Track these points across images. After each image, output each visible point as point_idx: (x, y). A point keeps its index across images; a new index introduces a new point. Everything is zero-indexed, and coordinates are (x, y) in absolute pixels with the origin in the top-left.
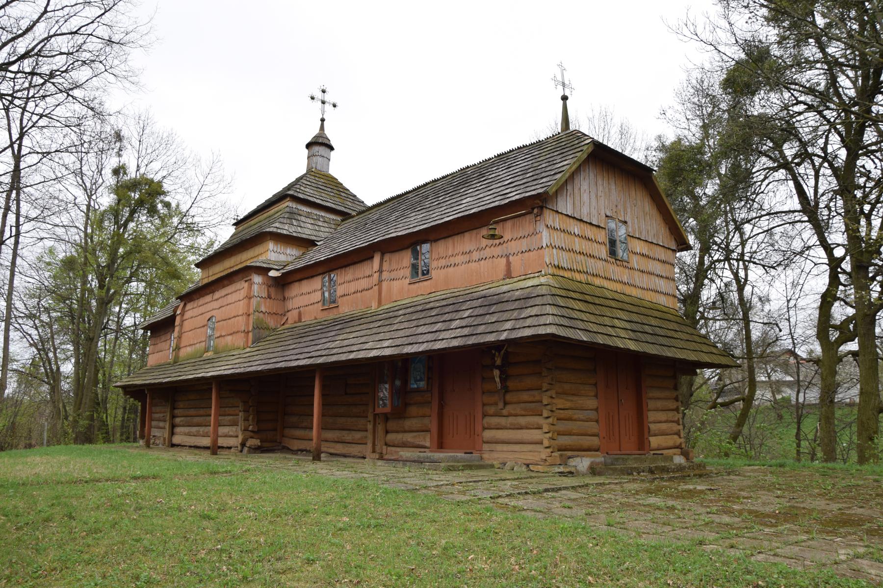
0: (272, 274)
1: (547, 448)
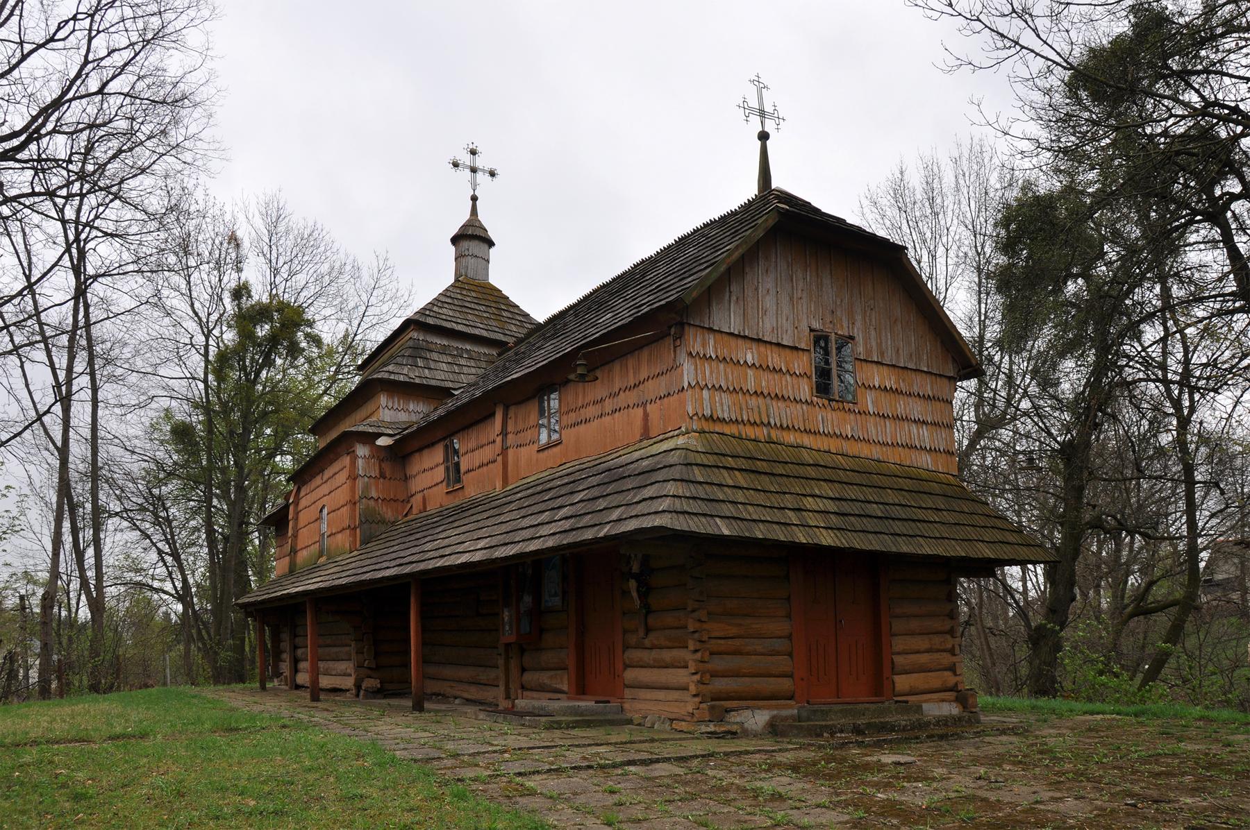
0: (382, 442)
1: (695, 696)
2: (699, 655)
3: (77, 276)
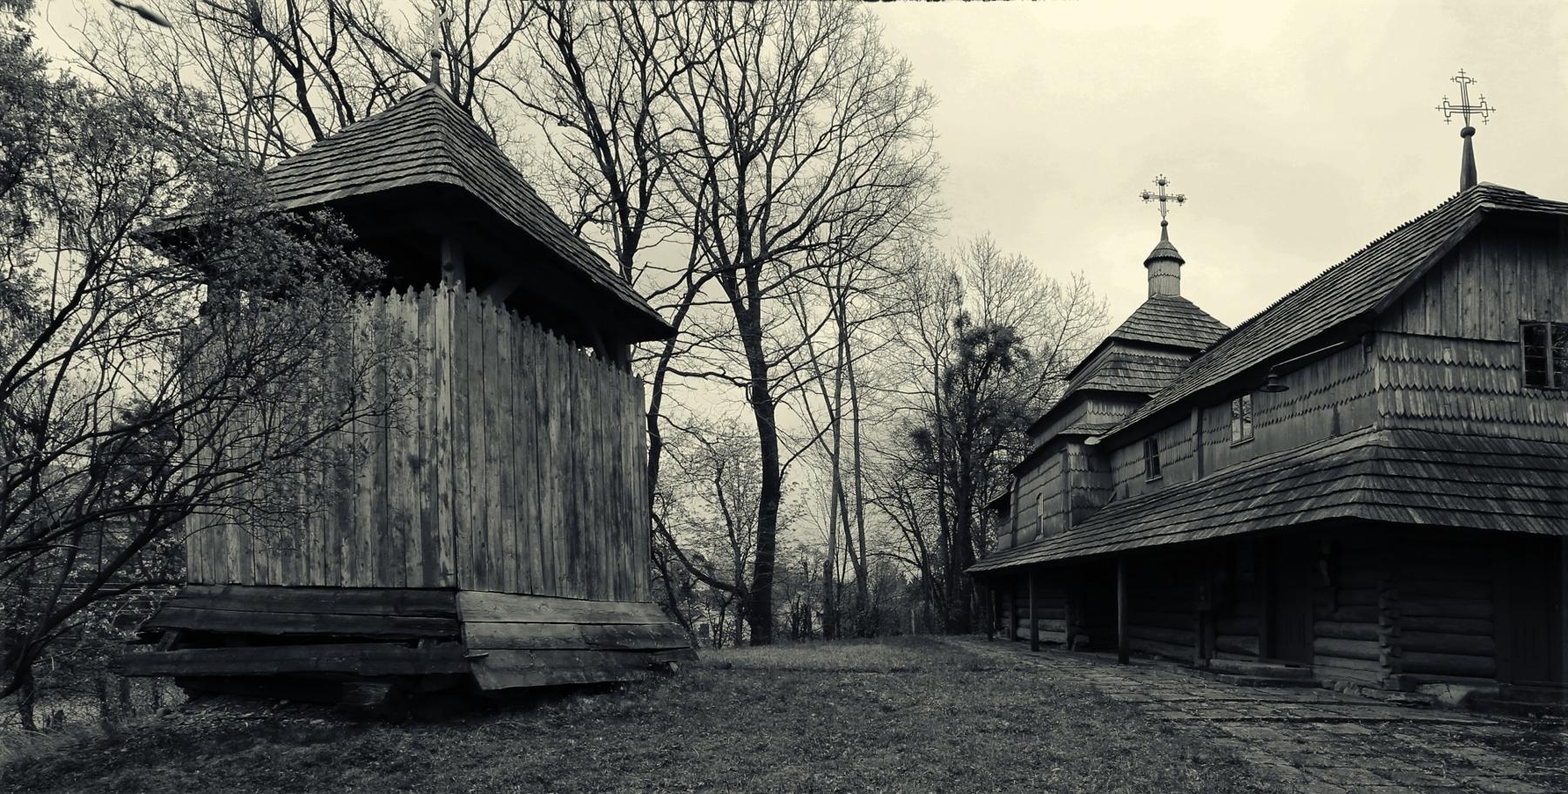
0: (1090, 441)
2: (1390, 630)
3: (840, 324)
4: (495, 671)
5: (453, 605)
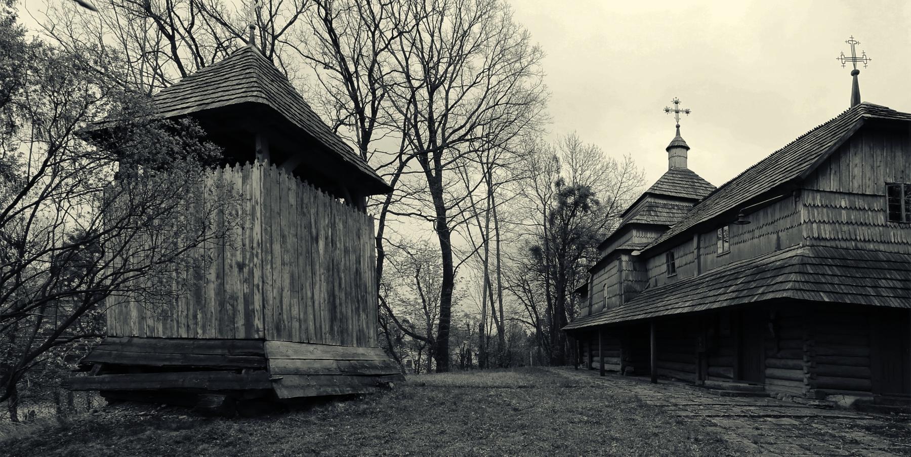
0: (634, 253)
2: (810, 364)
3: (488, 185)
4: (287, 387)
5: (263, 349)
